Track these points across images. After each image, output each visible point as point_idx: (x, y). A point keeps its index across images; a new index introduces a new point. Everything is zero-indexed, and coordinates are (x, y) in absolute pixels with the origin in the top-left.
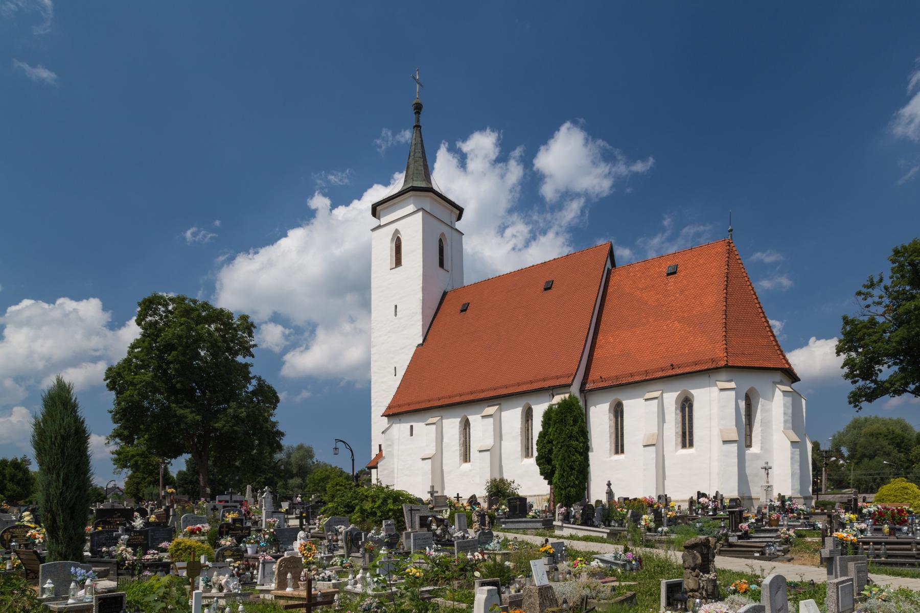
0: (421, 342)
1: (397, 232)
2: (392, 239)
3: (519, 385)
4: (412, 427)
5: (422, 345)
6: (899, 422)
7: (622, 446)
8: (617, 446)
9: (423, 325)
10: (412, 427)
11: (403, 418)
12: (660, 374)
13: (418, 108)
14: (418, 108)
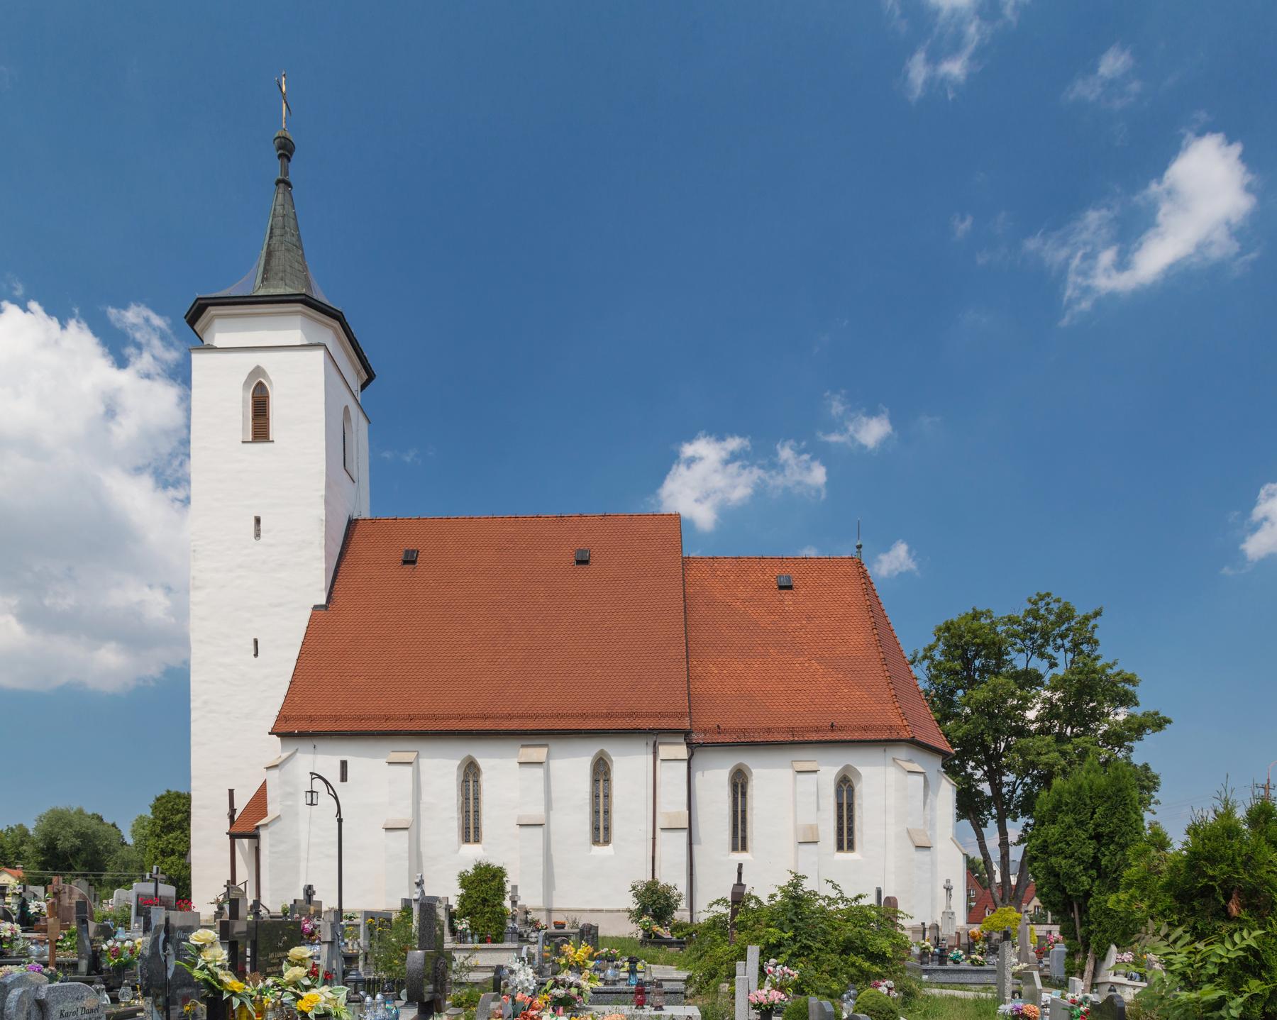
0: (322, 600)
1: (258, 371)
2: (246, 384)
3: (387, 718)
4: (344, 764)
5: (325, 607)
6: (52, 811)
7: (477, 829)
8: (596, 829)
9: (327, 570)
10: (344, 764)
11: (322, 745)
12: (814, 737)
13: (286, 150)
14: (286, 150)
